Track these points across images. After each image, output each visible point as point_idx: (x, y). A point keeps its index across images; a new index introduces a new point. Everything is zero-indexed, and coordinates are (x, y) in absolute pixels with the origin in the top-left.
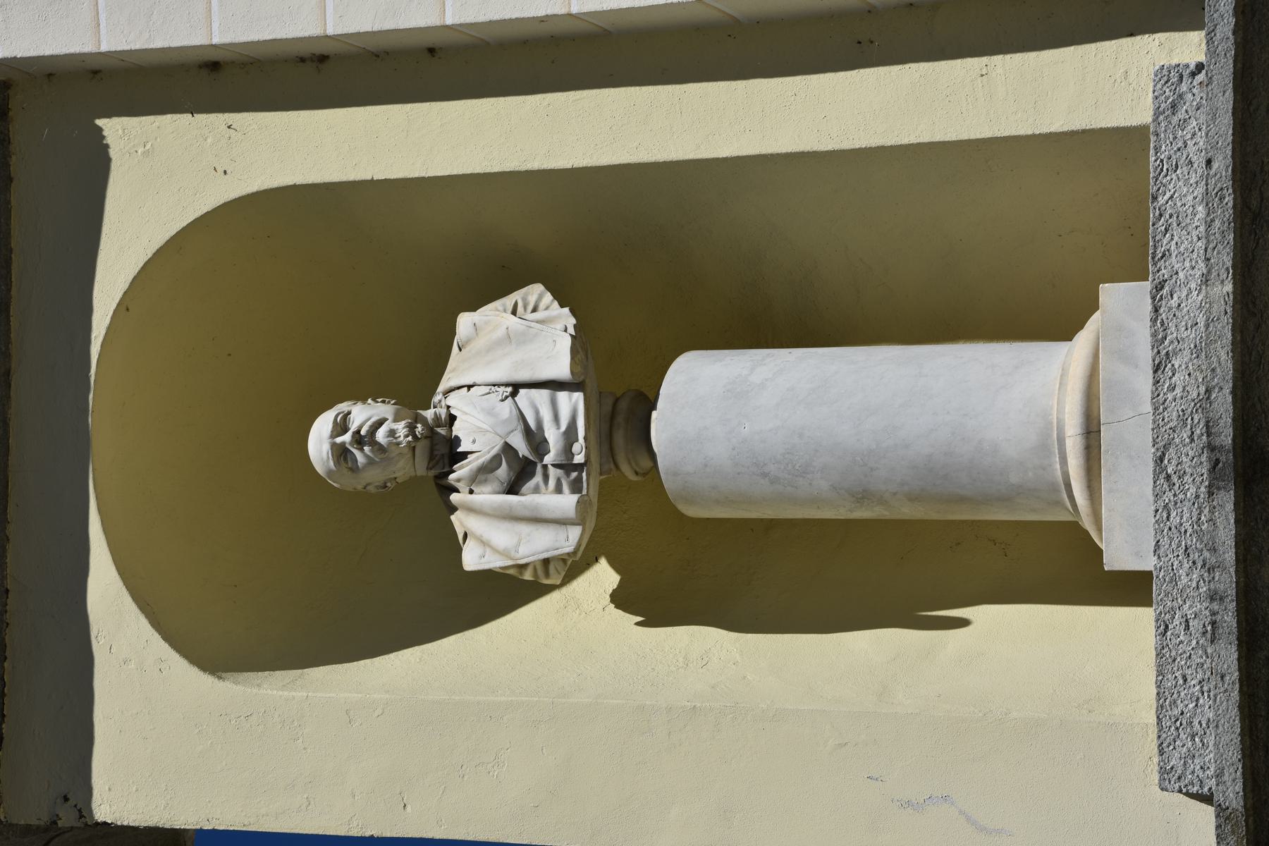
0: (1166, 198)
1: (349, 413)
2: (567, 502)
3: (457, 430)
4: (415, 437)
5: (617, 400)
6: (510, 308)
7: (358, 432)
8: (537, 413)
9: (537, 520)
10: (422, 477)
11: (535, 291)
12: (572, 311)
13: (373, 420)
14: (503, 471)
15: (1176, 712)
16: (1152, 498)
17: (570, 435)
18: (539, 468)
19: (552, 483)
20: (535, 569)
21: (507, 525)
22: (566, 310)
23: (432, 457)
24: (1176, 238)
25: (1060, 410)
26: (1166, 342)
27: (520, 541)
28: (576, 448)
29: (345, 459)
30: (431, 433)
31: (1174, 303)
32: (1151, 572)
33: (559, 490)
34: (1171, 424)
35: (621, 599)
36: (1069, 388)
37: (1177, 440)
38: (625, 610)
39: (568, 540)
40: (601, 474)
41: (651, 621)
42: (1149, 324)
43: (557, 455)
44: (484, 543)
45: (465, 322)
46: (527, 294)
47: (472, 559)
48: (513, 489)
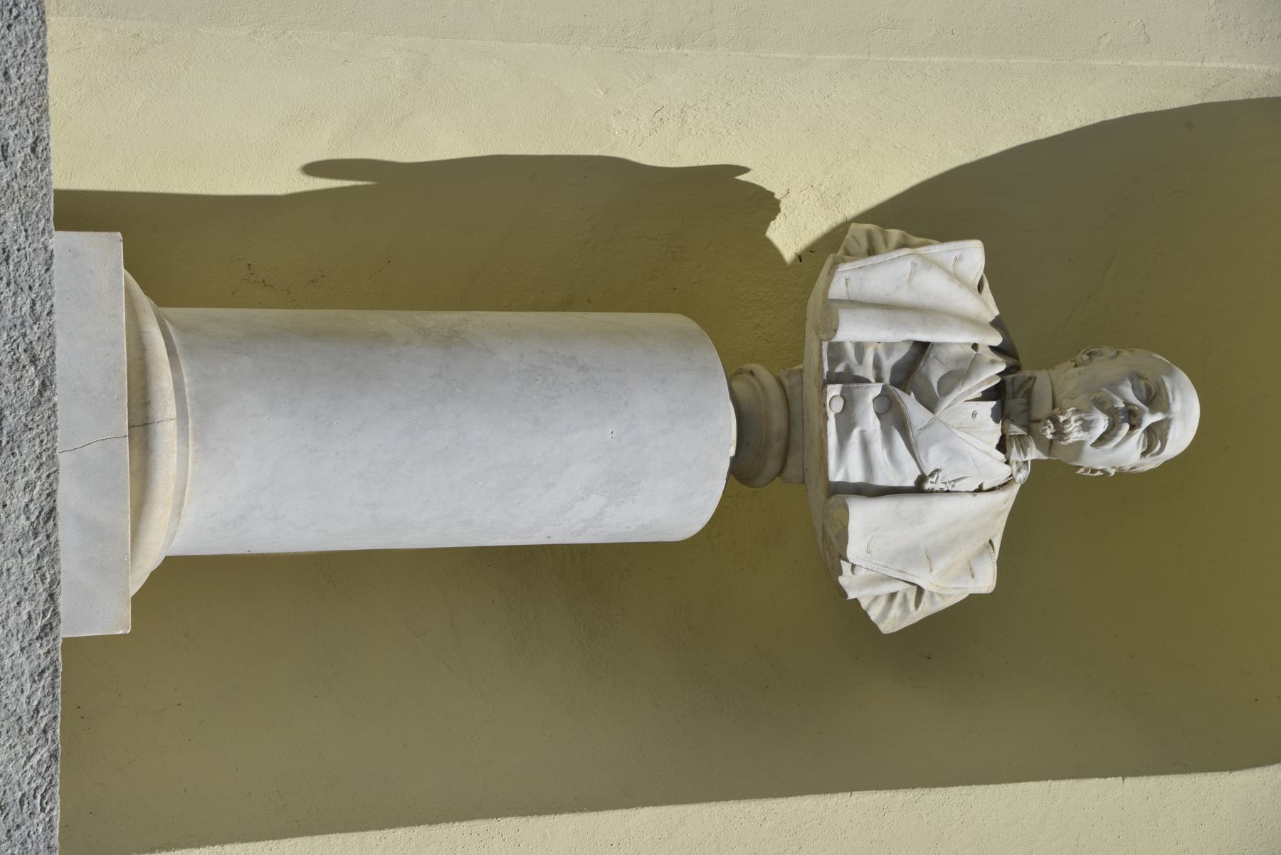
0: (37, 757)
1: (1144, 454)
2: (850, 331)
3: (994, 431)
4: (1055, 420)
5: (780, 472)
6: (925, 599)
7: (1133, 428)
8: (891, 454)
9: (888, 308)
10: (1039, 369)
11: (890, 621)
12: (845, 594)
13: (1112, 444)
14: (936, 373)
15: (18, 28)
16: (57, 332)
17: (847, 423)
18: (887, 377)
19: (869, 358)
20: (886, 242)
21: (928, 301)
22: (851, 596)
23: (1029, 394)
24: (23, 699)
25: (183, 457)
26: (37, 551)
27: (910, 279)
28: (838, 406)
29: (1149, 390)
30: (1031, 425)
31: (27, 608)
32: (57, 229)
33: (860, 348)
34: (30, 435)
35: (767, 205)
36: (172, 488)
37: (22, 412)
38: (761, 190)
39: (848, 279)
40: (801, 371)
41: (727, 175)
42: (62, 577)
43: (865, 395)
44: (956, 277)
45: (985, 580)
46: (902, 618)
47: (971, 256)
48: (922, 348)
